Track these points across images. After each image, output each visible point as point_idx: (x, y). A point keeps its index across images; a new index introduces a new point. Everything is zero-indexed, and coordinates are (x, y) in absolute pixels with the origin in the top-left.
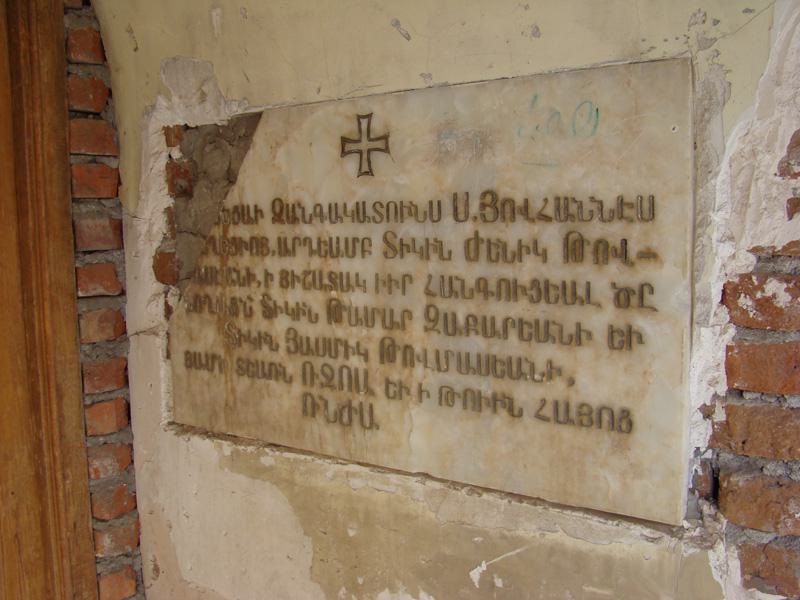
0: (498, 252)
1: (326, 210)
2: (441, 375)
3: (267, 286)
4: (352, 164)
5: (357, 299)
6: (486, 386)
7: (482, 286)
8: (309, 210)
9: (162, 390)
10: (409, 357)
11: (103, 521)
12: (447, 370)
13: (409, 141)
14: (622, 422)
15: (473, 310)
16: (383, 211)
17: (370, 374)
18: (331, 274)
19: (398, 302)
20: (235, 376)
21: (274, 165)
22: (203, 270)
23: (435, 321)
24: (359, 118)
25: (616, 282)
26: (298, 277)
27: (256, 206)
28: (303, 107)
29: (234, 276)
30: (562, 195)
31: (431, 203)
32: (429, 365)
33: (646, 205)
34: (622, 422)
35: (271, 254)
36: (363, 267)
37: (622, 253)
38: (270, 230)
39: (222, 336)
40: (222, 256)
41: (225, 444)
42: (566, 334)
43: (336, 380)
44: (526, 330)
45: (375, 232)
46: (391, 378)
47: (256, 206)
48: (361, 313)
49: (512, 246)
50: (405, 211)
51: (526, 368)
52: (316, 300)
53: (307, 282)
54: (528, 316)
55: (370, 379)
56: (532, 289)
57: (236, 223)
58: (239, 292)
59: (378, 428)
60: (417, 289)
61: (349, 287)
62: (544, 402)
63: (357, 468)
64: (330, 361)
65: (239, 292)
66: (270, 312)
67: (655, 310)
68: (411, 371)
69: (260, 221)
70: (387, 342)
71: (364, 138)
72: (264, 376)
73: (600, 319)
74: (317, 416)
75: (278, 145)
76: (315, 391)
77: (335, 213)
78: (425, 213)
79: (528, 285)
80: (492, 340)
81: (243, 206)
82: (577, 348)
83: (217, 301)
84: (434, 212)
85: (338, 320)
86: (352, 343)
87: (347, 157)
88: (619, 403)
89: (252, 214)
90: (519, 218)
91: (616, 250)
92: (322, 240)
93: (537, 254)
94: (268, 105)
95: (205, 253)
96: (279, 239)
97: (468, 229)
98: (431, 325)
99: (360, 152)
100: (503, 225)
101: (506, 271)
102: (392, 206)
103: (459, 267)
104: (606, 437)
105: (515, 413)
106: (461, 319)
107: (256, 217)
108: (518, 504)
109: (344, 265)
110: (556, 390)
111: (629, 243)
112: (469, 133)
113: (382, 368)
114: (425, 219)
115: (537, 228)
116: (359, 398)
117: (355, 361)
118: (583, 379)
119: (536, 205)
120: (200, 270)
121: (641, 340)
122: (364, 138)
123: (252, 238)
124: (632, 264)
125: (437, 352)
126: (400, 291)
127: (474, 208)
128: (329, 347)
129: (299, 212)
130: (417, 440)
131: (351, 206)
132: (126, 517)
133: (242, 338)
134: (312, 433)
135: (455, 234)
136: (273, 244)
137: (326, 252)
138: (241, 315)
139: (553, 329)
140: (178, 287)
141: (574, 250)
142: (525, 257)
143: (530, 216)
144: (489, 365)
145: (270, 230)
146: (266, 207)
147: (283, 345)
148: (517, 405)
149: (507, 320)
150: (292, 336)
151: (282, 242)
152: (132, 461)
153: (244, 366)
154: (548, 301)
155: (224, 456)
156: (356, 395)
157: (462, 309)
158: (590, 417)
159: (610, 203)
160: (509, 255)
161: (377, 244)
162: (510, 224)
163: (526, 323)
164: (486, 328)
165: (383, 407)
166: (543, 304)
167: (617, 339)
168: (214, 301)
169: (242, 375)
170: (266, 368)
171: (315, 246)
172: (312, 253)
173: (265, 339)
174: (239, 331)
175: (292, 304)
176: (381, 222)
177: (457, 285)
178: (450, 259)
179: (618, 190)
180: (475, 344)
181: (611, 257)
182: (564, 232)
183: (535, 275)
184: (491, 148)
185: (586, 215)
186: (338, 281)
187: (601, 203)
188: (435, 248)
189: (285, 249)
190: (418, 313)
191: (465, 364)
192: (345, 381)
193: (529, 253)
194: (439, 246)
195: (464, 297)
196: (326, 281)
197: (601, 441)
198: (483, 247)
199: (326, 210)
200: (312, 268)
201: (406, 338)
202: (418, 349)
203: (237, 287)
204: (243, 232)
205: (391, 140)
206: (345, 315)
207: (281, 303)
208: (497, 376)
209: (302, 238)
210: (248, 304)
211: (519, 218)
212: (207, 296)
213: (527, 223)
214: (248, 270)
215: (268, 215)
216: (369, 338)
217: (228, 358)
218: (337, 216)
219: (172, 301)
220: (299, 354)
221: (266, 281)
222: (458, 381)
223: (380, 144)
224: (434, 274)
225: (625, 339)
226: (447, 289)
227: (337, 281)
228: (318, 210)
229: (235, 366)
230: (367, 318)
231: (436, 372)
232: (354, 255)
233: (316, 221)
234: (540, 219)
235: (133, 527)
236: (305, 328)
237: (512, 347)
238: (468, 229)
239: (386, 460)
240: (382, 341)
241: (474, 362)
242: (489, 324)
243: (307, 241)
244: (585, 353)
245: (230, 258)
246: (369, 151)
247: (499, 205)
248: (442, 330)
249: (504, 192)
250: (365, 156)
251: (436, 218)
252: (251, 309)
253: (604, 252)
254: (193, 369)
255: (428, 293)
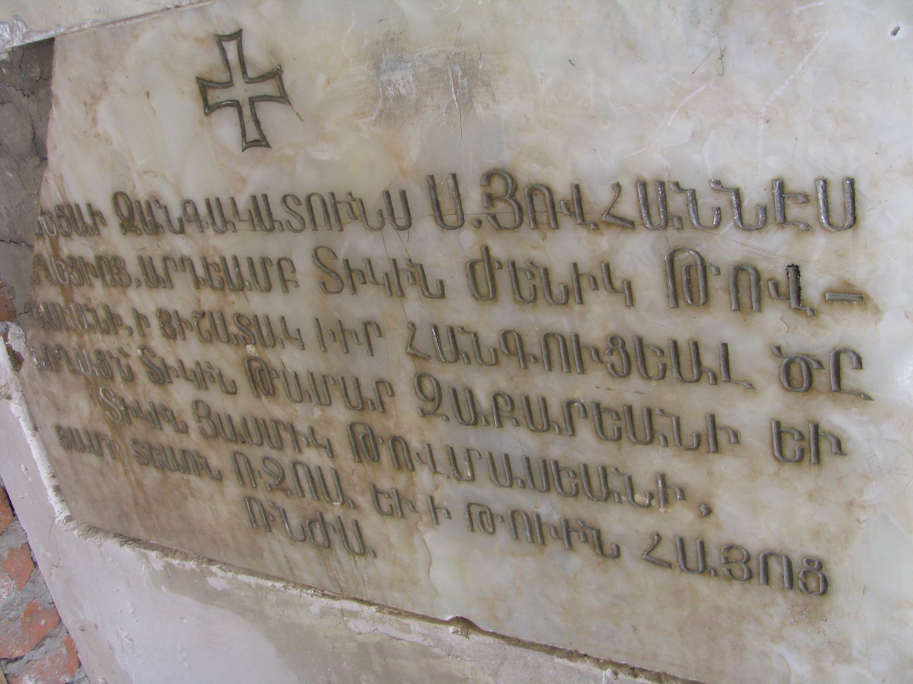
0: (532, 284)
1: (203, 210)
2: (465, 486)
3: (144, 336)
4: (226, 128)
5: (291, 359)
6: (549, 508)
7: (512, 345)
8: (176, 212)
9: (43, 477)
10: (402, 455)
11: (16, 659)
12: (473, 478)
13: (322, 78)
14: (809, 579)
15: (503, 385)
16: (303, 210)
17: (343, 475)
18: (239, 317)
19: (364, 368)
20: (136, 465)
21: (97, 135)
22: (42, 307)
23: (437, 399)
24: (220, 40)
25: (781, 342)
26: (187, 323)
27: (89, 206)
28: (118, 29)
29: (90, 318)
30: (647, 176)
31: (388, 194)
32: (439, 469)
33: (837, 197)
34: (809, 579)
35: (134, 284)
36: (294, 306)
37: (792, 288)
38: (126, 247)
39: (99, 408)
40: (62, 287)
41: (153, 554)
42: (686, 430)
43: (290, 481)
44: (609, 422)
45: (299, 249)
46: (378, 485)
47: (89, 206)
48: (306, 383)
49: (561, 273)
50: (343, 210)
51: (616, 483)
52: (226, 358)
53: (203, 331)
54: (607, 400)
55: (344, 485)
56: (611, 352)
57: (68, 235)
58: (105, 343)
59: (375, 556)
60: (393, 346)
61: (274, 341)
62: (658, 539)
63: (355, 606)
64: (274, 454)
65: (105, 343)
66: (161, 375)
67: (868, 398)
68: (411, 478)
69: (104, 231)
70: (359, 430)
71: (238, 78)
72: (178, 468)
73: (755, 410)
74: (274, 530)
75: (96, 99)
76: (262, 495)
77: (219, 215)
78: (381, 212)
79: (602, 346)
80: (548, 436)
81: (69, 206)
82: (711, 457)
83: (78, 355)
84: (395, 212)
85: (271, 392)
86: (302, 427)
87: (216, 116)
88: (801, 549)
89: (88, 220)
90: (566, 222)
91: (776, 286)
92: (210, 260)
93: (613, 289)
94: (59, 26)
95: (36, 282)
96: (141, 259)
97: (468, 241)
98: (430, 407)
99: (236, 104)
100: (536, 236)
101: (560, 321)
102: (316, 202)
103: (461, 310)
104: (779, 598)
105: (605, 550)
106: (484, 401)
107: (95, 224)
108: (631, 678)
109: (257, 304)
110: (680, 520)
111: (804, 273)
112: (434, 56)
113: (360, 469)
114: (383, 223)
115: (605, 241)
116: (334, 511)
117: (312, 457)
118: (728, 507)
119: (599, 196)
120: (38, 308)
121: (839, 447)
122: (238, 78)
123: (99, 258)
124: (814, 312)
125: (452, 453)
126: (364, 348)
127: (474, 202)
128: (269, 432)
129: (160, 216)
130: (442, 576)
131: (243, 202)
132: (48, 641)
133: (130, 412)
134: (272, 552)
135: (443, 253)
136: (133, 268)
137: (222, 282)
138: (119, 378)
139: (660, 422)
140: (19, 324)
141: (688, 282)
142: (590, 296)
143: (588, 217)
144: (548, 476)
145: (126, 247)
146: (105, 206)
147: (193, 424)
148: (609, 541)
149: (569, 404)
150: (202, 412)
151: (145, 264)
152: (35, 564)
153: (145, 451)
154: (647, 377)
155: (154, 570)
156: (328, 506)
157: (483, 384)
158: (749, 567)
159: (756, 194)
160: (558, 291)
161: (304, 265)
162: (550, 234)
163: (608, 410)
164: (535, 415)
165: (374, 526)
166: (636, 381)
167: (791, 446)
168: (72, 354)
169: (147, 464)
170: (178, 456)
171: (200, 271)
172: (198, 283)
173: (160, 415)
174: (123, 401)
175: (189, 364)
176: (301, 231)
177: (464, 342)
178: (443, 296)
179: (771, 167)
180: (516, 441)
181: (766, 300)
182: (664, 250)
183: (612, 327)
184: (486, 84)
185: (707, 216)
186: (254, 330)
187: (737, 192)
188: (408, 277)
189: (155, 277)
190: (404, 386)
191: (502, 470)
192: (305, 484)
193: (596, 287)
194: (418, 274)
195: (483, 363)
196: (233, 329)
197: (778, 605)
198: (504, 278)
199: (203, 210)
200: (206, 307)
201: (391, 424)
202: (415, 443)
203: (99, 335)
204: (78, 247)
205: (288, 78)
206: (278, 383)
207: (171, 361)
208: (564, 494)
209: (177, 257)
210: (123, 361)
211: (566, 222)
212: (59, 347)
213: (584, 233)
214: (107, 308)
215: (113, 222)
216: (329, 422)
217: (119, 440)
218: (225, 222)
219: (18, 346)
220: (221, 440)
221: (140, 326)
222: (486, 491)
223: (268, 88)
224: (417, 322)
225: (805, 448)
226: (447, 347)
227: (251, 330)
228: (189, 209)
229: (132, 451)
230: (318, 390)
231: (454, 481)
232: (269, 288)
233: (190, 229)
234: (608, 224)
235: (64, 650)
236: (216, 399)
237: (585, 448)
238: (468, 241)
239: (396, 598)
240: (352, 426)
241: (519, 470)
242: (535, 409)
243: (185, 263)
244: (727, 466)
245: (75, 289)
246: (253, 101)
247: (522, 196)
248: (451, 416)
249: (529, 171)
250: (246, 110)
251: (402, 222)
252: (129, 368)
253: (750, 288)
254: (74, 451)
255: (416, 355)
